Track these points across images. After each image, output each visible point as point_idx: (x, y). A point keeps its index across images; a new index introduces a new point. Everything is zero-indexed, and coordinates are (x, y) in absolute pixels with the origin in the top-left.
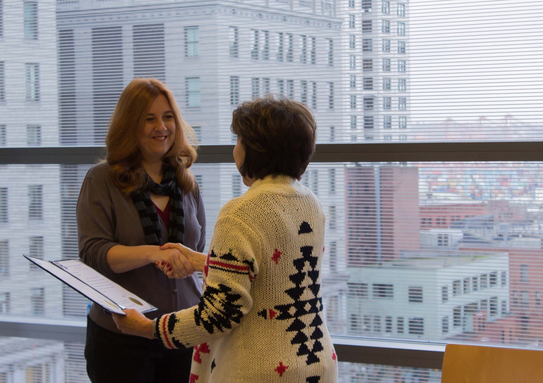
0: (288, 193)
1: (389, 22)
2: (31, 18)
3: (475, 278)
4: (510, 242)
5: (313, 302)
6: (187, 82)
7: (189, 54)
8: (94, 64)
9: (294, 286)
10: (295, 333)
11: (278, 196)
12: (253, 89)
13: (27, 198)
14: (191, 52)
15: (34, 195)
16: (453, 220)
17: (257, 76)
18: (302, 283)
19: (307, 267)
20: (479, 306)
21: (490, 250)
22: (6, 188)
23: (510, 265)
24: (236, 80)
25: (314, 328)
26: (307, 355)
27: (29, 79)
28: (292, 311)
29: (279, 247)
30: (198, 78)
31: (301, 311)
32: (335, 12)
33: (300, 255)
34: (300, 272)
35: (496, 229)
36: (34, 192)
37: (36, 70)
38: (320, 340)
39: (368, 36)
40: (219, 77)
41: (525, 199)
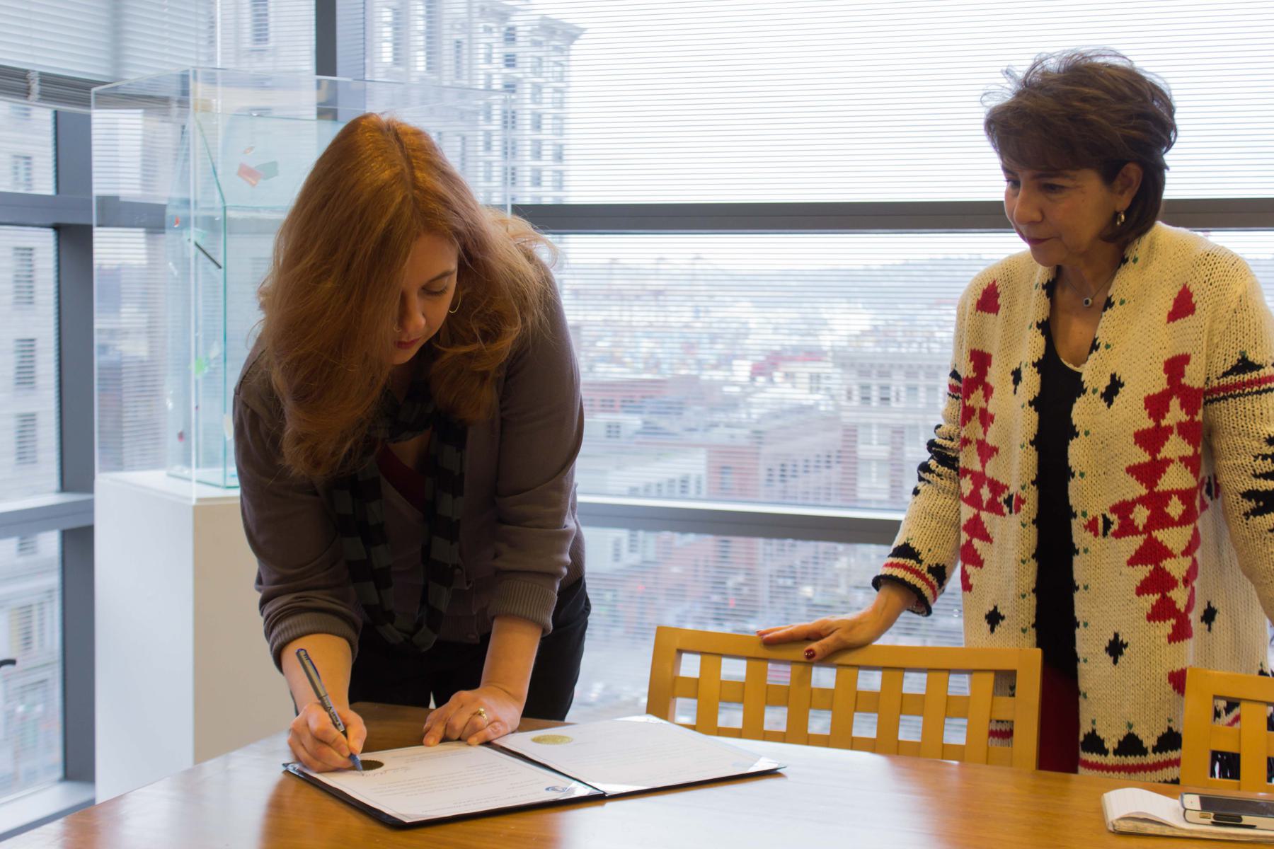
1: (540, 116)
3: (659, 485)
9: (1145, 457)
26: (1173, 621)
28: (1141, 515)
31: (1159, 520)
34: (1158, 425)
41: (718, 375)
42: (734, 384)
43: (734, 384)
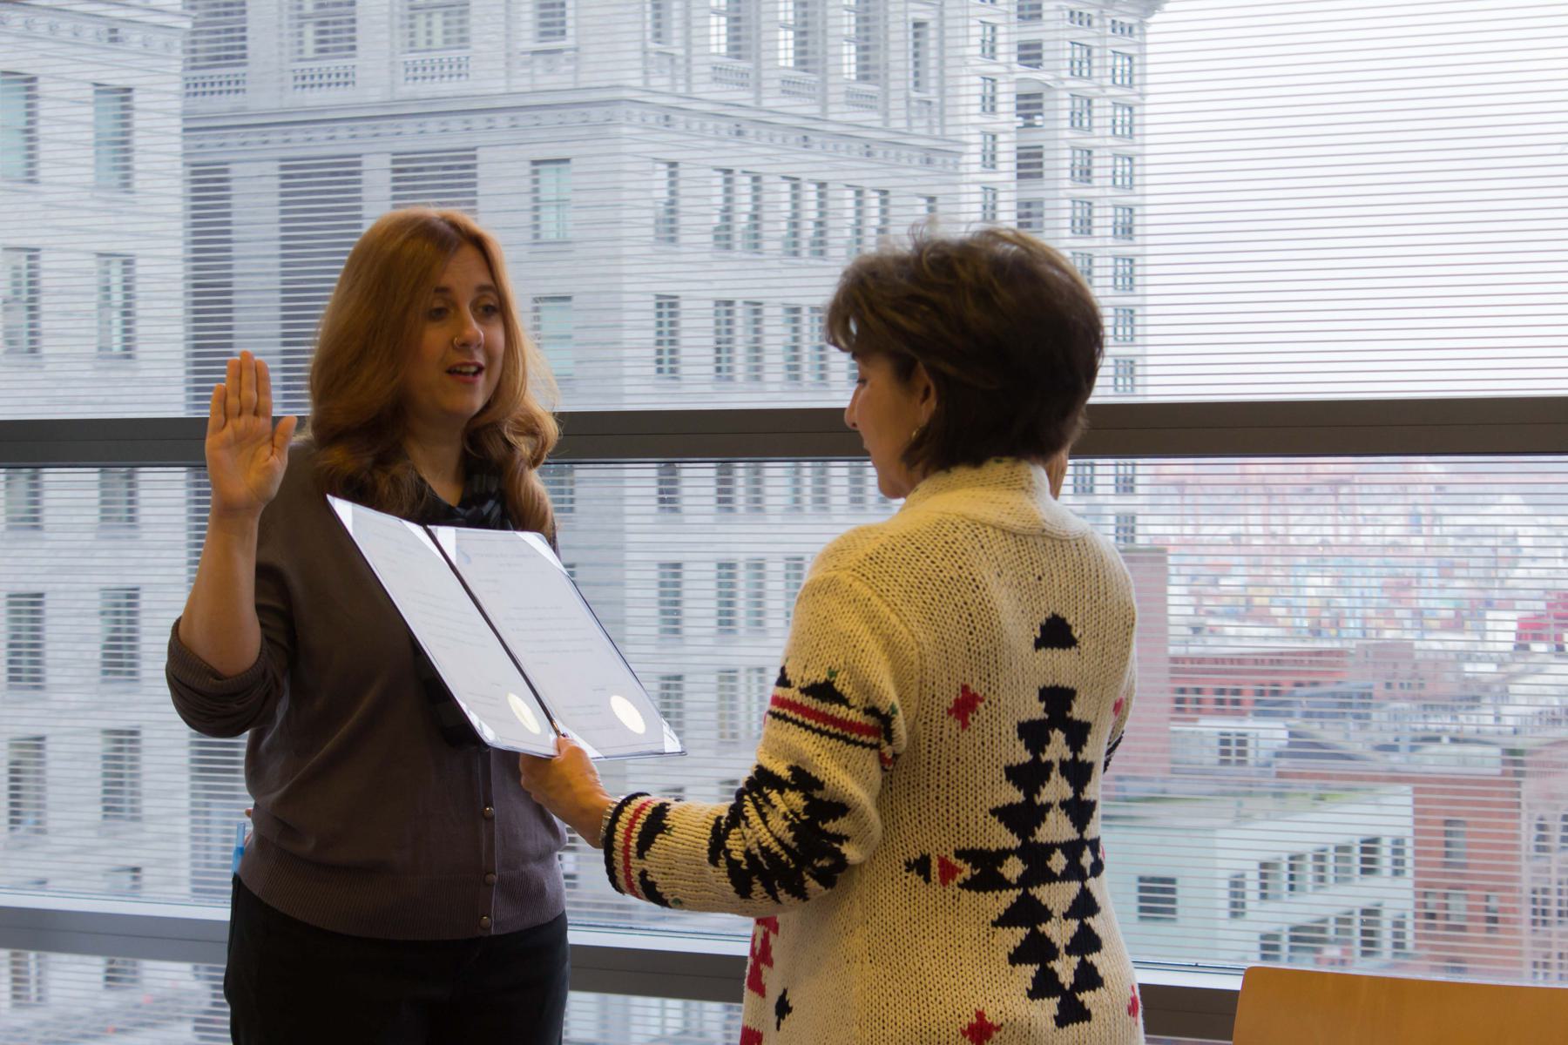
0: (1020, 524)
2: (115, 134)
4: (1415, 757)
5: (1073, 850)
6: (537, 310)
7: (544, 237)
8: (284, 256)
9: (1018, 797)
10: (1021, 933)
11: (990, 530)
12: (718, 332)
13: (97, 621)
14: (549, 231)
15: (118, 613)
16: (1262, 693)
17: (727, 296)
18: (1043, 791)
19: (1057, 748)
20: (1331, 928)
21: (1360, 778)
22: (40, 595)
23: (1416, 822)
24: (672, 305)
25: (1074, 924)
26: (1058, 999)
27: (108, 297)
28: (1013, 869)
29: (976, 679)
30: (567, 299)
31: (1038, 873)
32: (943, 125)
33: (1037, 711)
34: (1036, 759)
35: (1381, 724)
36: (118, 605)
37: (125, 271)
38: (1094, 958)
39: (1032, 191)
40: (626, 297)
41: (1455, 642)
42: (1486, 657)
43: (1486, 657)
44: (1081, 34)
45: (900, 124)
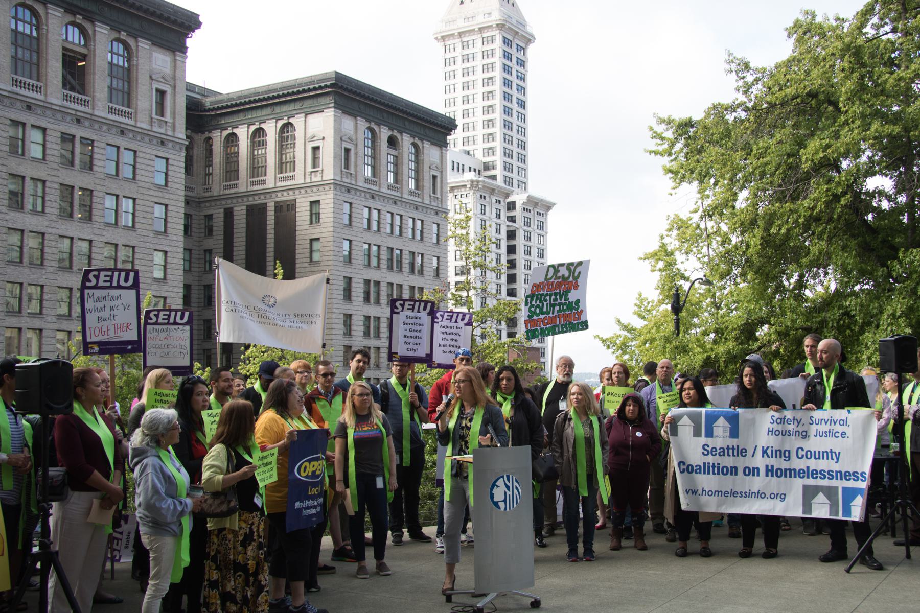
44: (527, 214)
45: (428, 202)
